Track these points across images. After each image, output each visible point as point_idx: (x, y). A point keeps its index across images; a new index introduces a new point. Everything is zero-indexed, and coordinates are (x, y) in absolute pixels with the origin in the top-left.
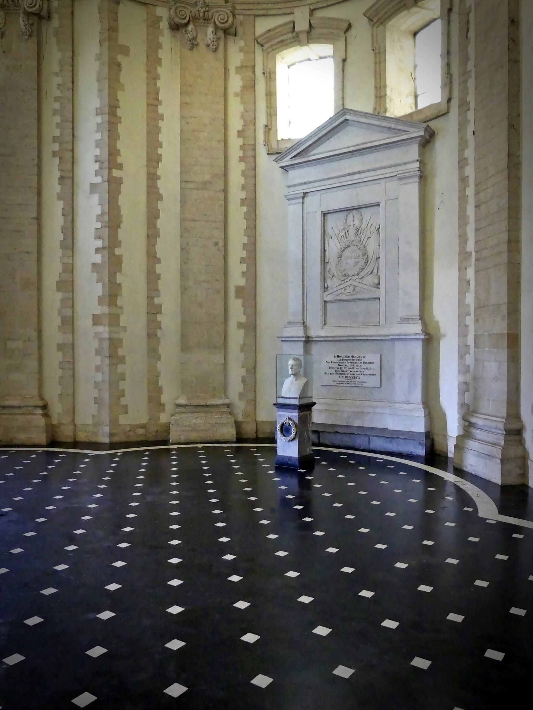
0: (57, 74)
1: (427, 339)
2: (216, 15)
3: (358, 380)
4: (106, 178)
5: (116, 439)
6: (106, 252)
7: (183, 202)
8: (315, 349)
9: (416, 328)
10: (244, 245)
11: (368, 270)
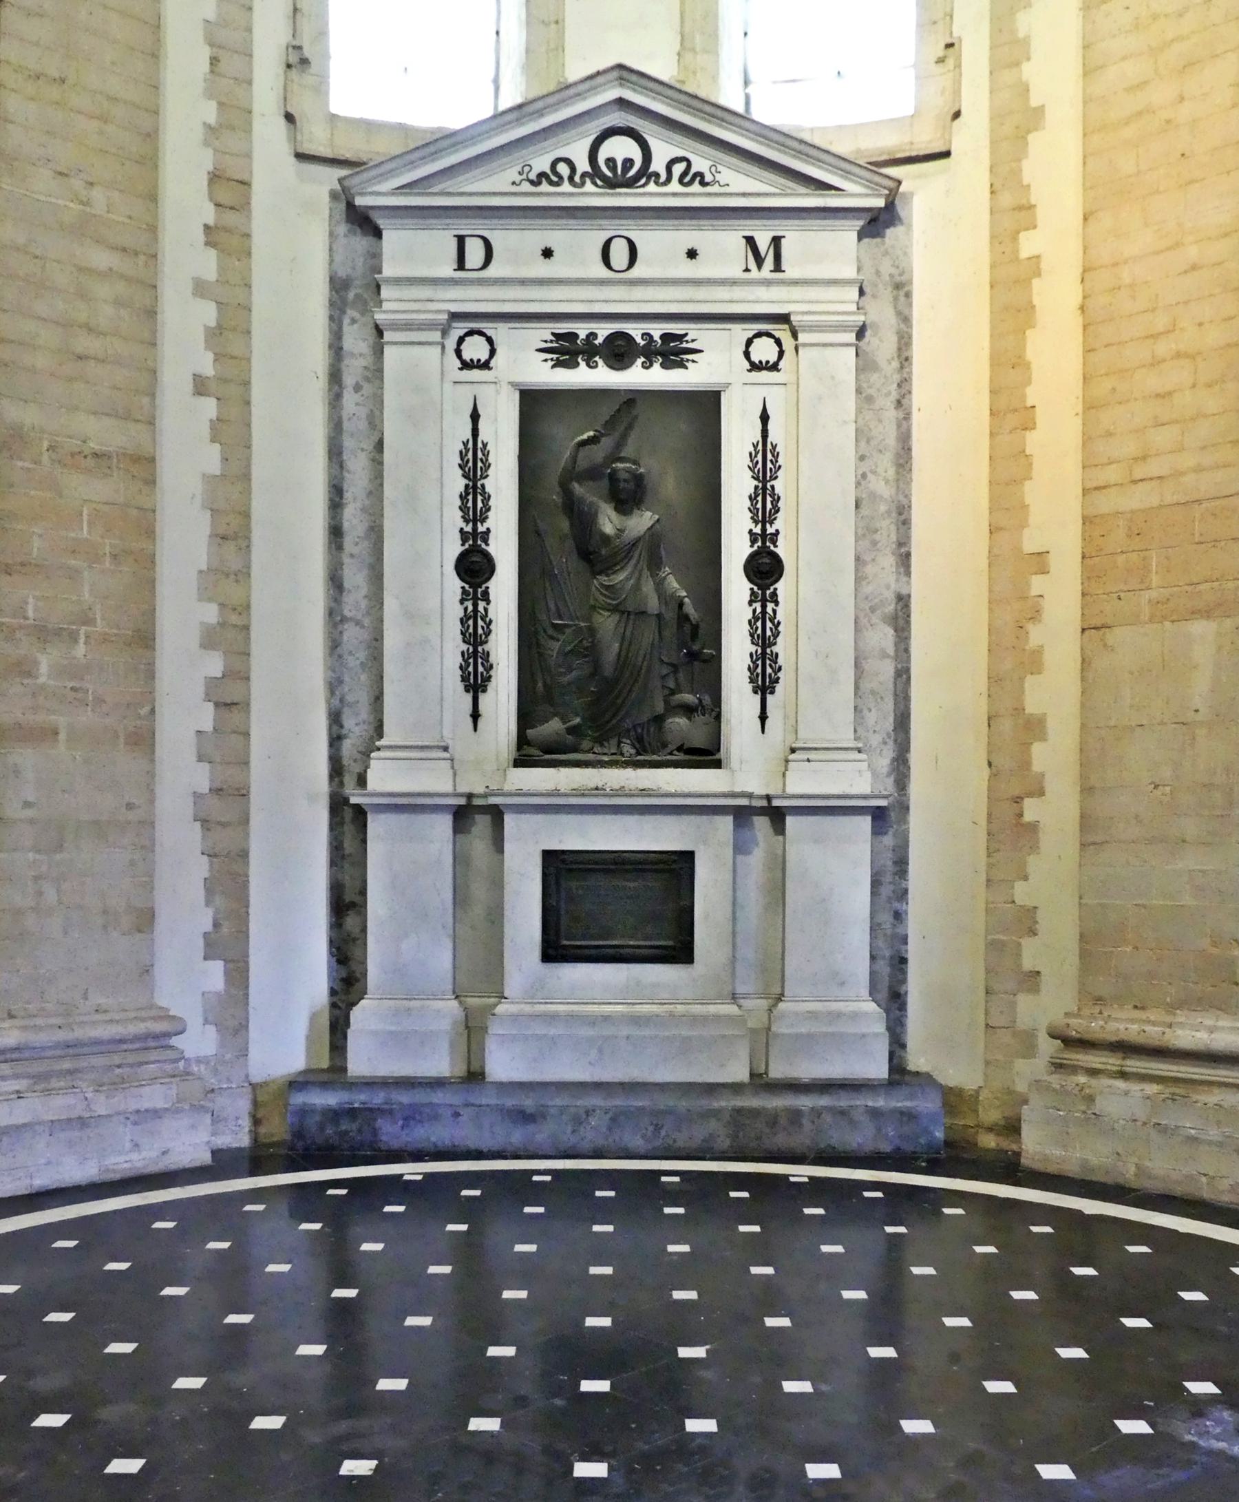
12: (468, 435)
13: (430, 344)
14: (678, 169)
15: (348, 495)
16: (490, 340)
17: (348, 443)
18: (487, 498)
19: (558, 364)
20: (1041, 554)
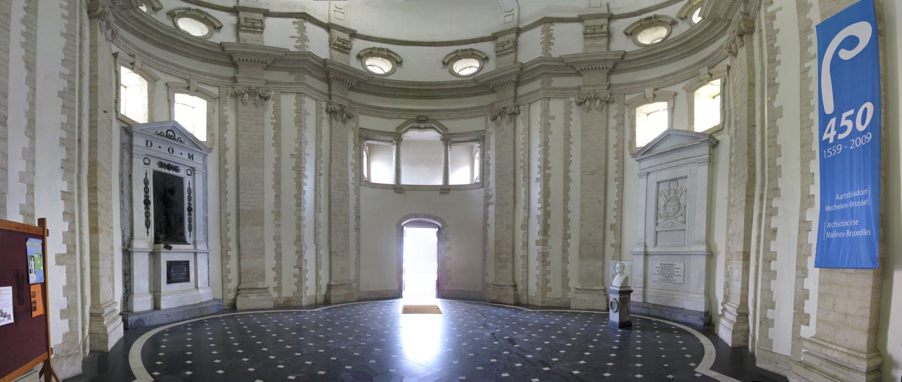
0: (522, 134)
1: (709, 255)
2: (601, 96)
3: (671, 278)
4: (543, 174)
5: (545, 304)
6: (542, 210)
7: (582, 182)
8: (650, 258)
9: (703, 248)
10: (616, 201)
11: (680, 213)
12: (145, 177)
13: (140, 158)
14: (179, 139)
15: (124, 185)
16: (149, 160)
17: (124, 175)
18: (145, 190)
19: (160, 167)
20: (229, 213)
